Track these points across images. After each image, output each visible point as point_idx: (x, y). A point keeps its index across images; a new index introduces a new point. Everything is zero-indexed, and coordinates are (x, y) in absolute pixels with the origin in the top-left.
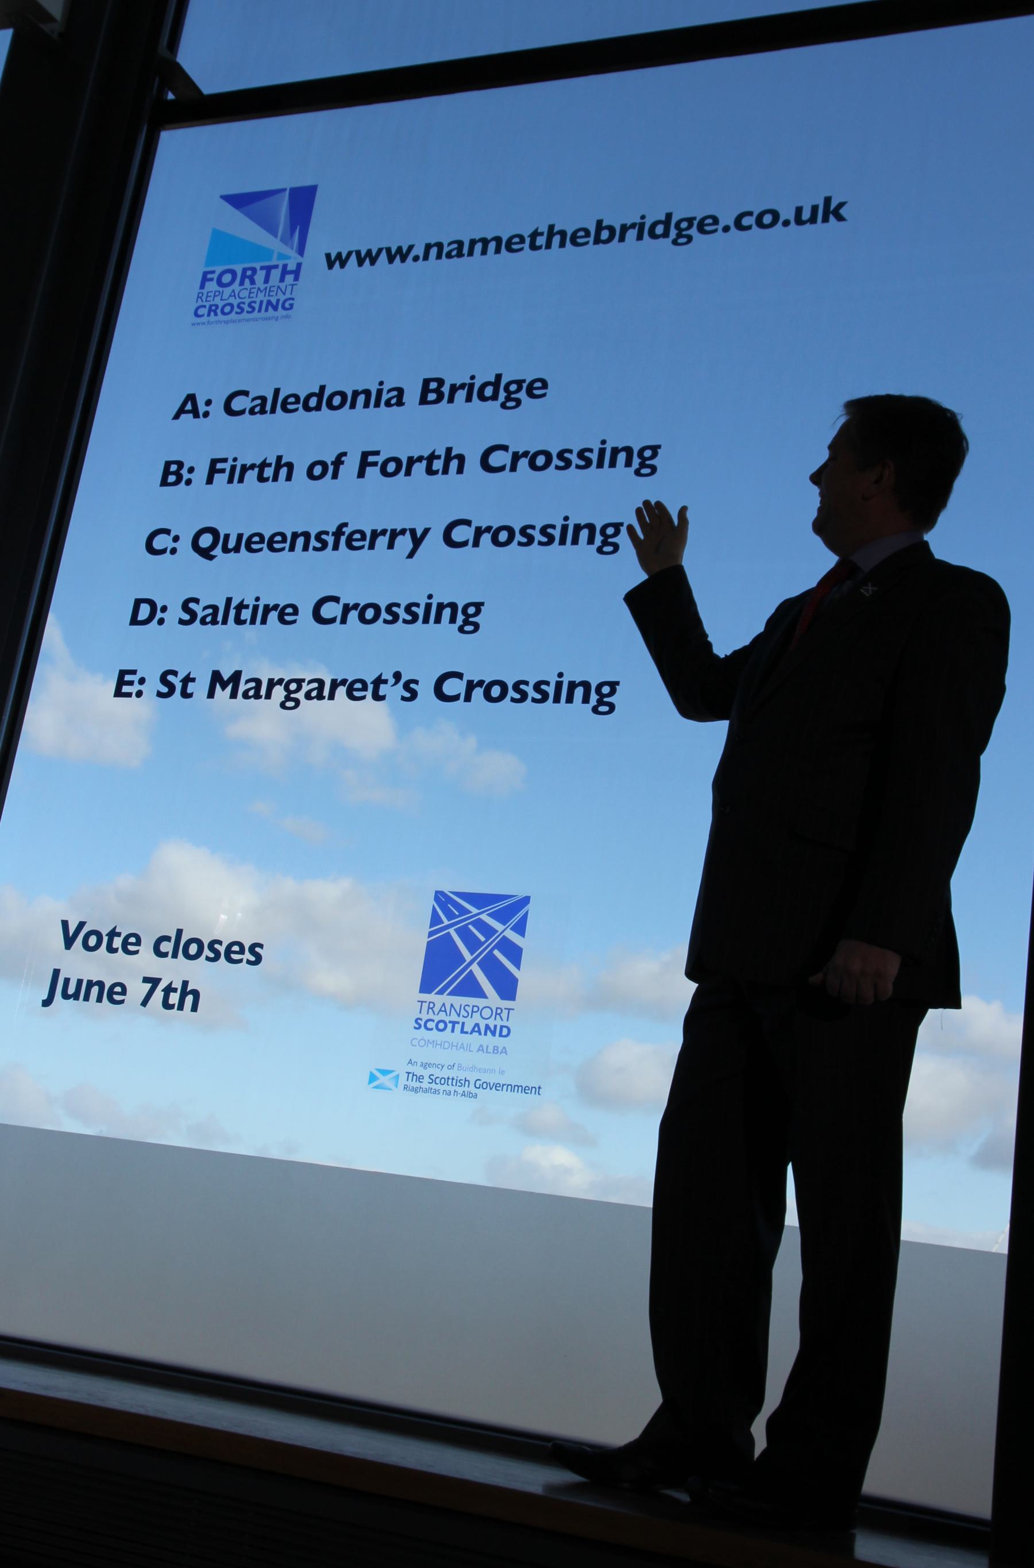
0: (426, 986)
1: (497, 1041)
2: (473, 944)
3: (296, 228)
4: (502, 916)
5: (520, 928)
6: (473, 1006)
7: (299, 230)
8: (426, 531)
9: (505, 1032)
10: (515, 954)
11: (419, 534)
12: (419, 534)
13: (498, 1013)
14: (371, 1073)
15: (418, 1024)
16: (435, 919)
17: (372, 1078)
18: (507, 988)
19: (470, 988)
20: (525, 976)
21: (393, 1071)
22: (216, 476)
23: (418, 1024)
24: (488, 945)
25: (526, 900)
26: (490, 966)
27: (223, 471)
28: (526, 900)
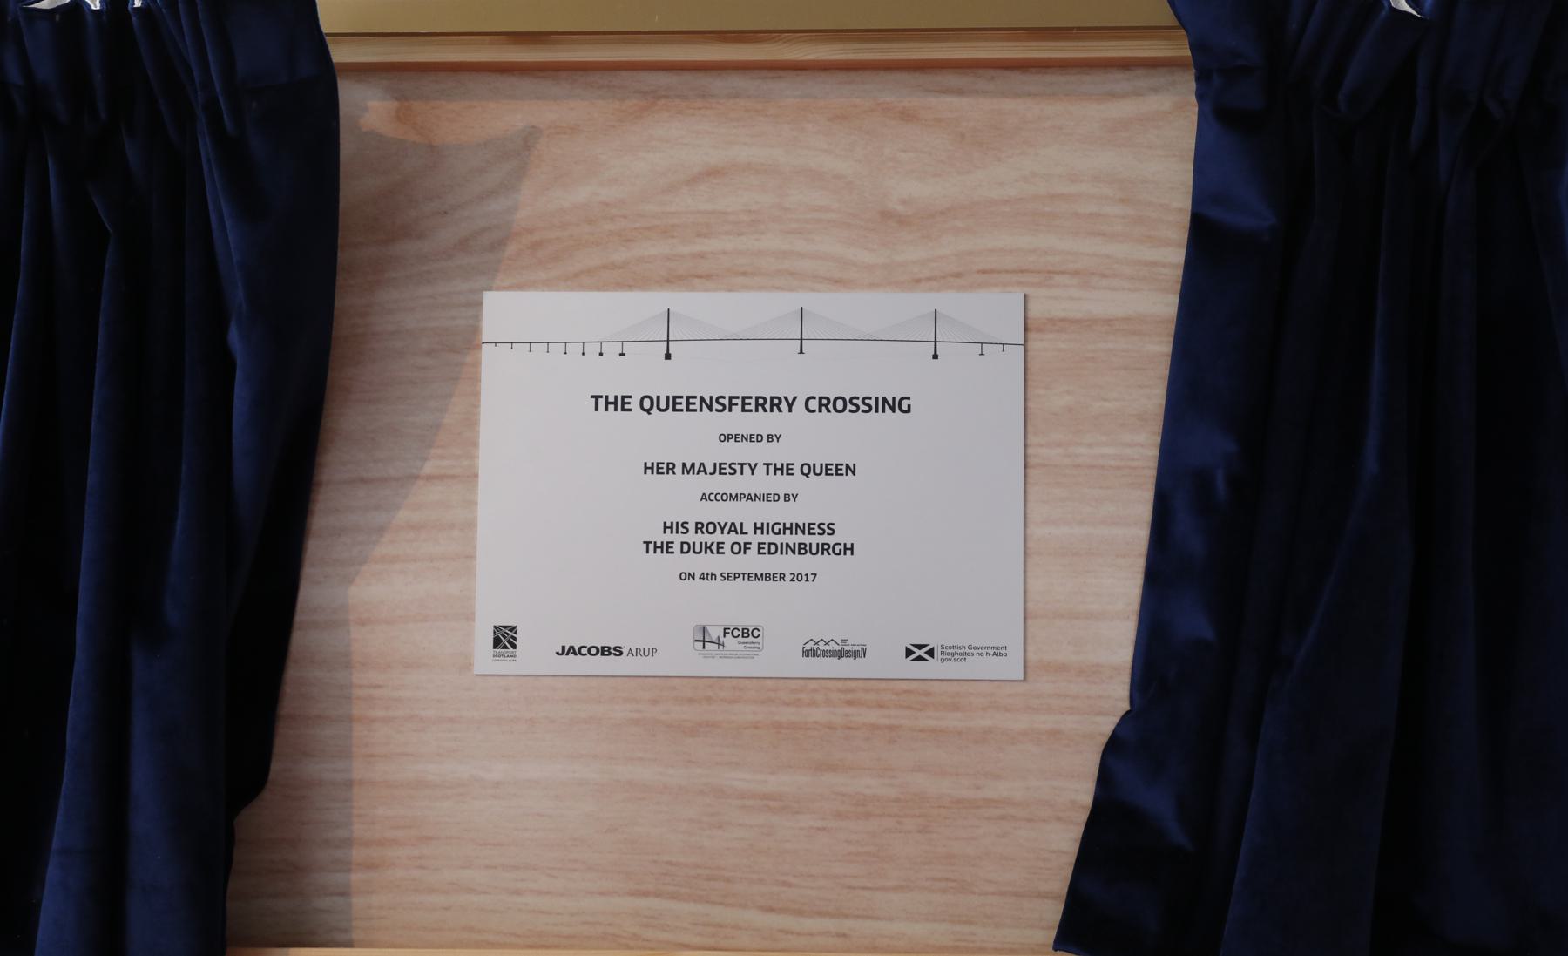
0: (495, 647)
1: (513, 658)
2: (505, 637)
3: (1414, 9)
4: (511, 630)
5: (515, 633)
6: (743, 629)
7: (1410, 14)
8: (756, 464)
9: (515, 656)
10: (515, 639)
11: (753, 466)
12: (753, 466)
13: (513, 652)
14: (907, 649)
15: (494, 656)
16: (495, 632)
17: (909, 652)
18: (514, 646)
19: (505, 647)
20: (517, 643)
21: (926, 646)
22: (733, 407)
23: (494, 656)
24: (508, 637)
25: (516, 627)
26: (509, 642)
27: (736, 404)
28: (516, 627)
